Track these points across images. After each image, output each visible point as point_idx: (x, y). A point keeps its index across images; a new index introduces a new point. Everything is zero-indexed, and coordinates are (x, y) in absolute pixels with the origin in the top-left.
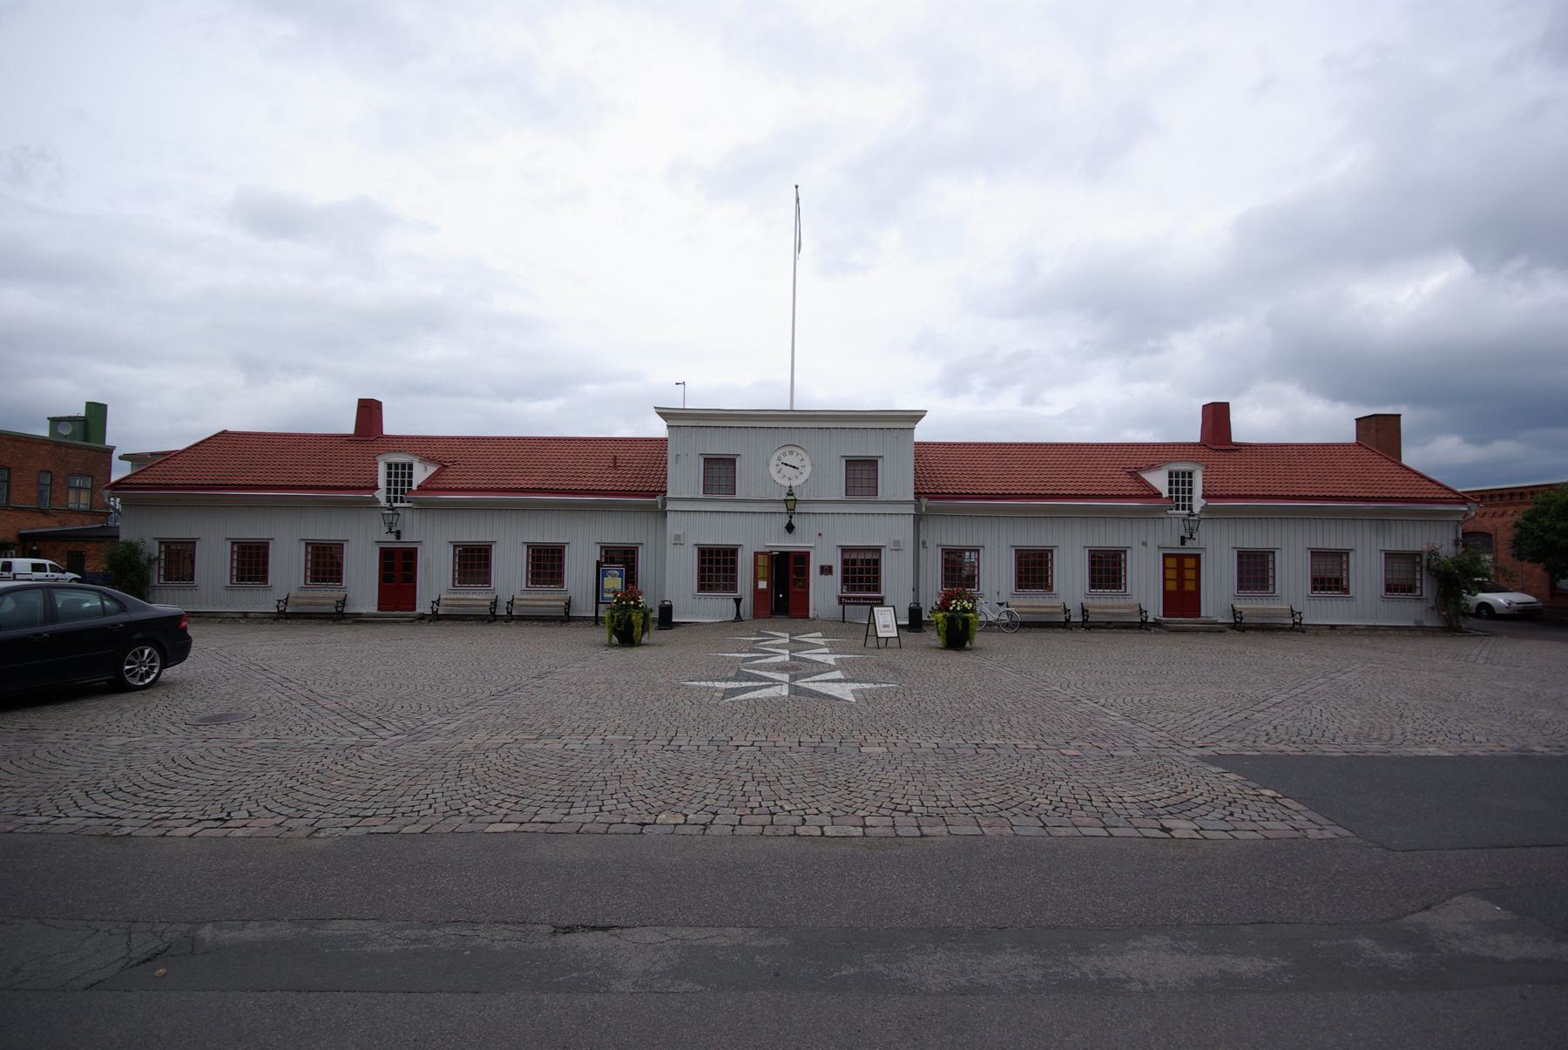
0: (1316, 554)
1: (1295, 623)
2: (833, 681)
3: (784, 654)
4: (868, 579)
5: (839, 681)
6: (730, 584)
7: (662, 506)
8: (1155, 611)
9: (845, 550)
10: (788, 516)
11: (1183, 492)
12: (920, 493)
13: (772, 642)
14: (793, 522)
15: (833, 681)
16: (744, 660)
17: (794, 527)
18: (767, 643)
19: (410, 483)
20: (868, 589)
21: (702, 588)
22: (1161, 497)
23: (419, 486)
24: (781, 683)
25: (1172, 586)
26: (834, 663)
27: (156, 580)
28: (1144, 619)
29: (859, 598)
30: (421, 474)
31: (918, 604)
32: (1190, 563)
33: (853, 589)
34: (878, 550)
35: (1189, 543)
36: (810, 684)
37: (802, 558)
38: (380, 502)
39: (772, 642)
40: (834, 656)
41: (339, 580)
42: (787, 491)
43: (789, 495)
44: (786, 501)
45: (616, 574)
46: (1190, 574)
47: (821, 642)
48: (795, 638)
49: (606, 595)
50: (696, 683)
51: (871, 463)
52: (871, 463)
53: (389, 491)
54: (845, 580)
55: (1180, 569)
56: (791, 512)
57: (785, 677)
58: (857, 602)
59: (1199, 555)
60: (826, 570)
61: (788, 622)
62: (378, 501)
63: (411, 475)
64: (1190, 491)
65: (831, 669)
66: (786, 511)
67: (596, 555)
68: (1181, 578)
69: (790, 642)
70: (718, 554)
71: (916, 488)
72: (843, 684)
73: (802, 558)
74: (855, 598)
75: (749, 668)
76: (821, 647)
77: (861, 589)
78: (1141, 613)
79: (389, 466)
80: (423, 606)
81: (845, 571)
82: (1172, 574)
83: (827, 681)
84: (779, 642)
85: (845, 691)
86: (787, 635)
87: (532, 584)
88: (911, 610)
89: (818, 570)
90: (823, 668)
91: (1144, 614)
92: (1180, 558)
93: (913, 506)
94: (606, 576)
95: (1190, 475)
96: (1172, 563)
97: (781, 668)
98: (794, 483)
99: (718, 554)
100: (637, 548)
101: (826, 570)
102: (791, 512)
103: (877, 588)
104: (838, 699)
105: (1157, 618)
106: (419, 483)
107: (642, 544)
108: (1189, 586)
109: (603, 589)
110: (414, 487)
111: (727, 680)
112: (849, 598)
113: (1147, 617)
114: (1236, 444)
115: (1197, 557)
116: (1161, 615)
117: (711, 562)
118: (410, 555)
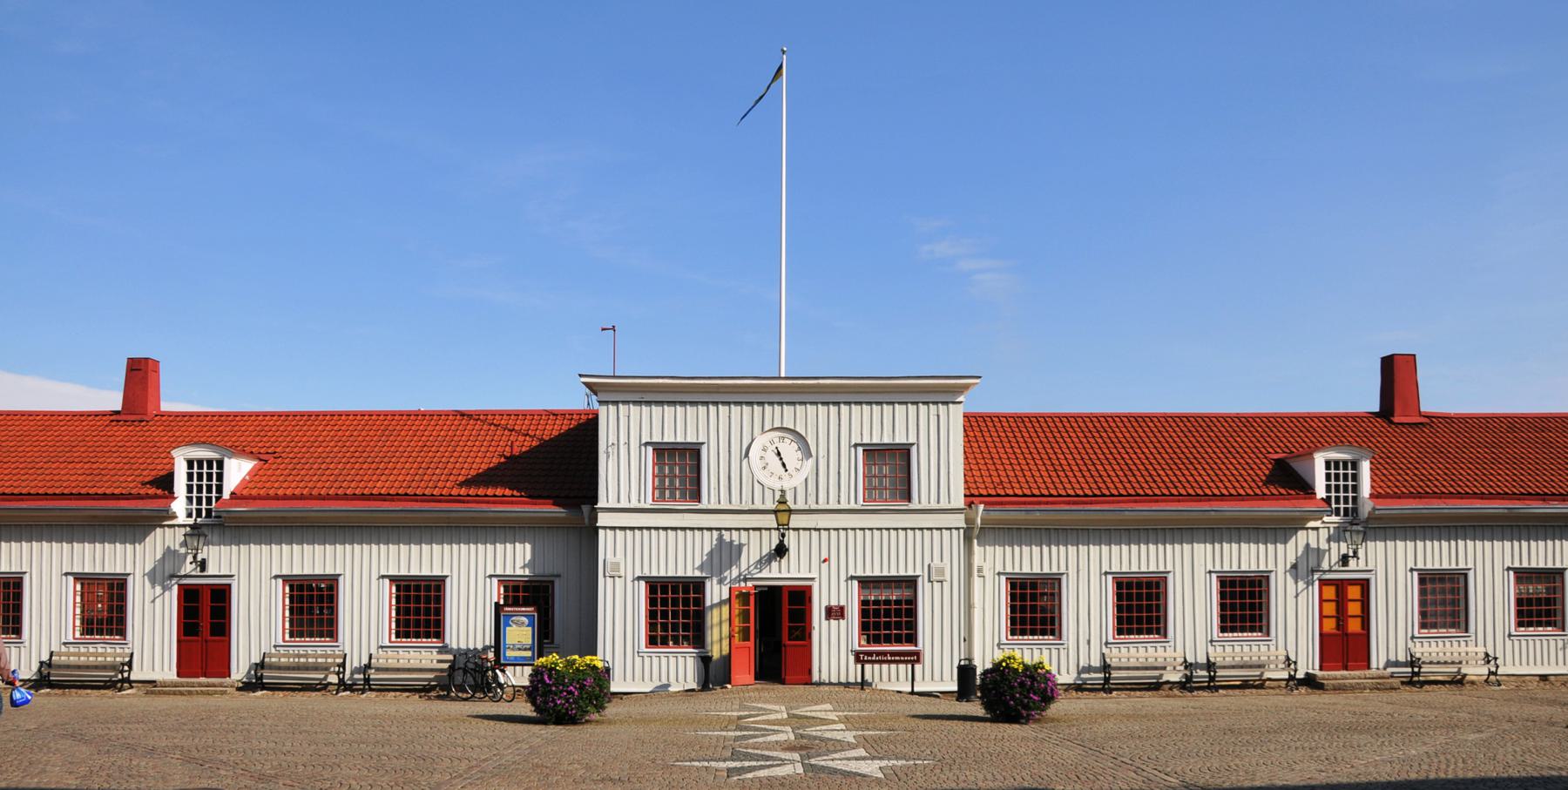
0: (1524, 575)
1: (1491, 673)
2: (857, 759)
3: (786, 732)
4: (898, 626)
5: (864, 759)
6: (696, 636)
7: (590, 519)
8: (1308, 662)
9: (865, 583)
10: (775, 534)
11: (1346, 490)
12: (972, 495)
13: (764, 717)
14: (786, 543)
15: (857, 759)
16: (737, 739)
17: (787, 550)
18: (758, 718)
19: (220, 489)
20: (899, 640)
21: (652, 641)
22: (1315, 498)
23: (232, 493)
24: (792, 762)
25: (1330, 625)
26: (854, 741)
27: (72, 636)
28: (1292, 673)
29: (884, 653)
30: (237, 471)
31: (970, 660)
32: (1354, 592)
33: (876, 640)
34: (911, 582)
35: (1352, 564)
36: (828, 762)
37: (800, 596)
38: (176, 517)
39: (764, 717)
40: (854, 733)
41: (122, 632)
42: (777, 498)
43: (780, 502)
44: (775, 512)
45: (523, 623)
46: (1354, 609)
47: (832, 716)
48: (795, 712)
49: (510, 654)
50: (688, 763)
51: (902, 454)
52: (902, 454)
53: (190, 499)
54: (864, 627)
55: (1341, 601)
56: (783, 528)
57: (796, 756)
58: (882, 658)
59: (1368, 581)
60: (835, 613)
61: (780, 688)
62: (174, 517)
63: (220, 477)
64: (1355, 489)
65: (851, 747)
66: (776, 526)
67: (495, 593)
68: (1341, 616)
69: (789, 717)
70: (675, 591)
71: (968, 488)
72: (867, 762)
73: (800, 596)
74: (878, 653)
75: (746, 748)
76: (834, 722)
77: (888, 640)
78: (1289, 665)
79: (190, 463)
80: (240, 669)
81: (864, 613)
82: (1330, 609)
83: (849, 759)
84: (772, 717)
85: (871, 768)
86: (783, 708)
87: (291, 637)
88: (960, 668)
89: (848, 612)
90: (841, 746)
91: (1292, 666)
92: (1341, 586)
93: (962, 516)
94: (510, 626)
95: (1355, 465)
96: (1330, 592)
97: (791, 748)
98: (787, 484)
99: (675, 591)
100: (553, 582)
101: (835, 613)
102: (783, 528)
103: (912, 639)
104: (864, 776)
105: (1311, 671)
106: (232, 490)
107: (559, 576)
108: (1354, 626)
109: (505, 644)
110: (226, 495)
111: (725, 760)
112: (870, 654)
113: (1296, 671)
114: (1429, 416)
115: (1365, 585)
116: (1317, 666)
117: (664, 602)
118: (220, 596)
